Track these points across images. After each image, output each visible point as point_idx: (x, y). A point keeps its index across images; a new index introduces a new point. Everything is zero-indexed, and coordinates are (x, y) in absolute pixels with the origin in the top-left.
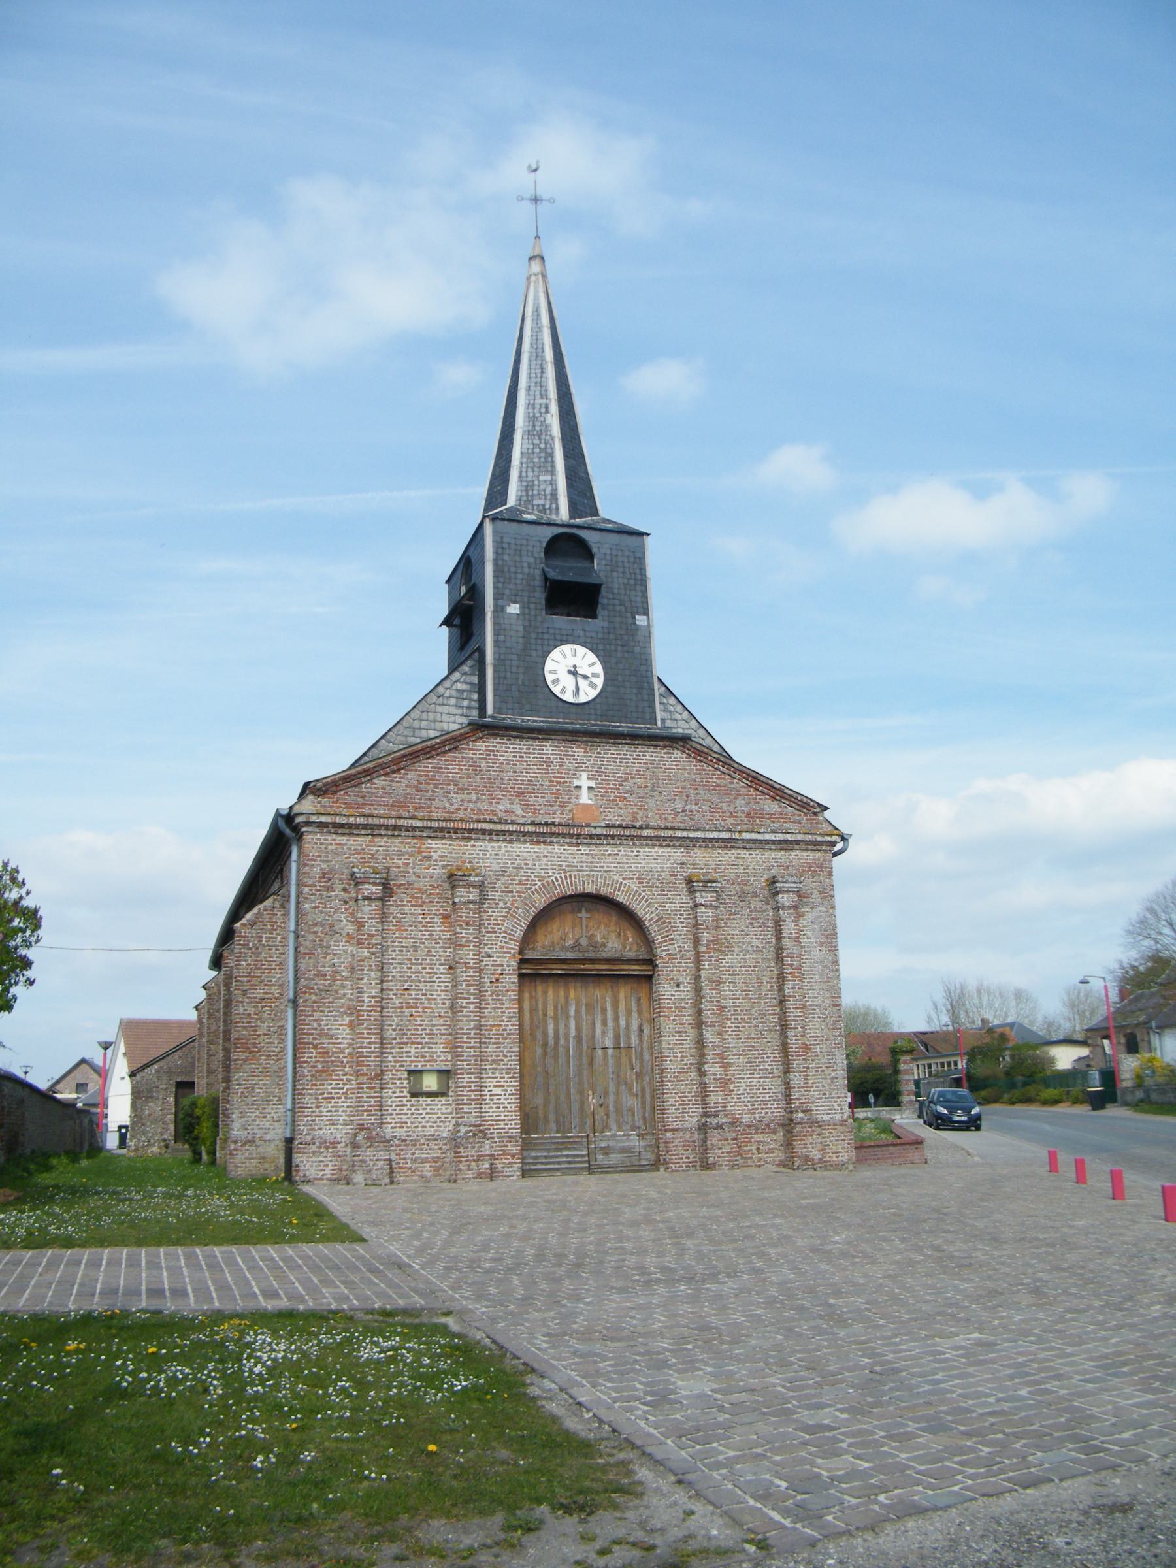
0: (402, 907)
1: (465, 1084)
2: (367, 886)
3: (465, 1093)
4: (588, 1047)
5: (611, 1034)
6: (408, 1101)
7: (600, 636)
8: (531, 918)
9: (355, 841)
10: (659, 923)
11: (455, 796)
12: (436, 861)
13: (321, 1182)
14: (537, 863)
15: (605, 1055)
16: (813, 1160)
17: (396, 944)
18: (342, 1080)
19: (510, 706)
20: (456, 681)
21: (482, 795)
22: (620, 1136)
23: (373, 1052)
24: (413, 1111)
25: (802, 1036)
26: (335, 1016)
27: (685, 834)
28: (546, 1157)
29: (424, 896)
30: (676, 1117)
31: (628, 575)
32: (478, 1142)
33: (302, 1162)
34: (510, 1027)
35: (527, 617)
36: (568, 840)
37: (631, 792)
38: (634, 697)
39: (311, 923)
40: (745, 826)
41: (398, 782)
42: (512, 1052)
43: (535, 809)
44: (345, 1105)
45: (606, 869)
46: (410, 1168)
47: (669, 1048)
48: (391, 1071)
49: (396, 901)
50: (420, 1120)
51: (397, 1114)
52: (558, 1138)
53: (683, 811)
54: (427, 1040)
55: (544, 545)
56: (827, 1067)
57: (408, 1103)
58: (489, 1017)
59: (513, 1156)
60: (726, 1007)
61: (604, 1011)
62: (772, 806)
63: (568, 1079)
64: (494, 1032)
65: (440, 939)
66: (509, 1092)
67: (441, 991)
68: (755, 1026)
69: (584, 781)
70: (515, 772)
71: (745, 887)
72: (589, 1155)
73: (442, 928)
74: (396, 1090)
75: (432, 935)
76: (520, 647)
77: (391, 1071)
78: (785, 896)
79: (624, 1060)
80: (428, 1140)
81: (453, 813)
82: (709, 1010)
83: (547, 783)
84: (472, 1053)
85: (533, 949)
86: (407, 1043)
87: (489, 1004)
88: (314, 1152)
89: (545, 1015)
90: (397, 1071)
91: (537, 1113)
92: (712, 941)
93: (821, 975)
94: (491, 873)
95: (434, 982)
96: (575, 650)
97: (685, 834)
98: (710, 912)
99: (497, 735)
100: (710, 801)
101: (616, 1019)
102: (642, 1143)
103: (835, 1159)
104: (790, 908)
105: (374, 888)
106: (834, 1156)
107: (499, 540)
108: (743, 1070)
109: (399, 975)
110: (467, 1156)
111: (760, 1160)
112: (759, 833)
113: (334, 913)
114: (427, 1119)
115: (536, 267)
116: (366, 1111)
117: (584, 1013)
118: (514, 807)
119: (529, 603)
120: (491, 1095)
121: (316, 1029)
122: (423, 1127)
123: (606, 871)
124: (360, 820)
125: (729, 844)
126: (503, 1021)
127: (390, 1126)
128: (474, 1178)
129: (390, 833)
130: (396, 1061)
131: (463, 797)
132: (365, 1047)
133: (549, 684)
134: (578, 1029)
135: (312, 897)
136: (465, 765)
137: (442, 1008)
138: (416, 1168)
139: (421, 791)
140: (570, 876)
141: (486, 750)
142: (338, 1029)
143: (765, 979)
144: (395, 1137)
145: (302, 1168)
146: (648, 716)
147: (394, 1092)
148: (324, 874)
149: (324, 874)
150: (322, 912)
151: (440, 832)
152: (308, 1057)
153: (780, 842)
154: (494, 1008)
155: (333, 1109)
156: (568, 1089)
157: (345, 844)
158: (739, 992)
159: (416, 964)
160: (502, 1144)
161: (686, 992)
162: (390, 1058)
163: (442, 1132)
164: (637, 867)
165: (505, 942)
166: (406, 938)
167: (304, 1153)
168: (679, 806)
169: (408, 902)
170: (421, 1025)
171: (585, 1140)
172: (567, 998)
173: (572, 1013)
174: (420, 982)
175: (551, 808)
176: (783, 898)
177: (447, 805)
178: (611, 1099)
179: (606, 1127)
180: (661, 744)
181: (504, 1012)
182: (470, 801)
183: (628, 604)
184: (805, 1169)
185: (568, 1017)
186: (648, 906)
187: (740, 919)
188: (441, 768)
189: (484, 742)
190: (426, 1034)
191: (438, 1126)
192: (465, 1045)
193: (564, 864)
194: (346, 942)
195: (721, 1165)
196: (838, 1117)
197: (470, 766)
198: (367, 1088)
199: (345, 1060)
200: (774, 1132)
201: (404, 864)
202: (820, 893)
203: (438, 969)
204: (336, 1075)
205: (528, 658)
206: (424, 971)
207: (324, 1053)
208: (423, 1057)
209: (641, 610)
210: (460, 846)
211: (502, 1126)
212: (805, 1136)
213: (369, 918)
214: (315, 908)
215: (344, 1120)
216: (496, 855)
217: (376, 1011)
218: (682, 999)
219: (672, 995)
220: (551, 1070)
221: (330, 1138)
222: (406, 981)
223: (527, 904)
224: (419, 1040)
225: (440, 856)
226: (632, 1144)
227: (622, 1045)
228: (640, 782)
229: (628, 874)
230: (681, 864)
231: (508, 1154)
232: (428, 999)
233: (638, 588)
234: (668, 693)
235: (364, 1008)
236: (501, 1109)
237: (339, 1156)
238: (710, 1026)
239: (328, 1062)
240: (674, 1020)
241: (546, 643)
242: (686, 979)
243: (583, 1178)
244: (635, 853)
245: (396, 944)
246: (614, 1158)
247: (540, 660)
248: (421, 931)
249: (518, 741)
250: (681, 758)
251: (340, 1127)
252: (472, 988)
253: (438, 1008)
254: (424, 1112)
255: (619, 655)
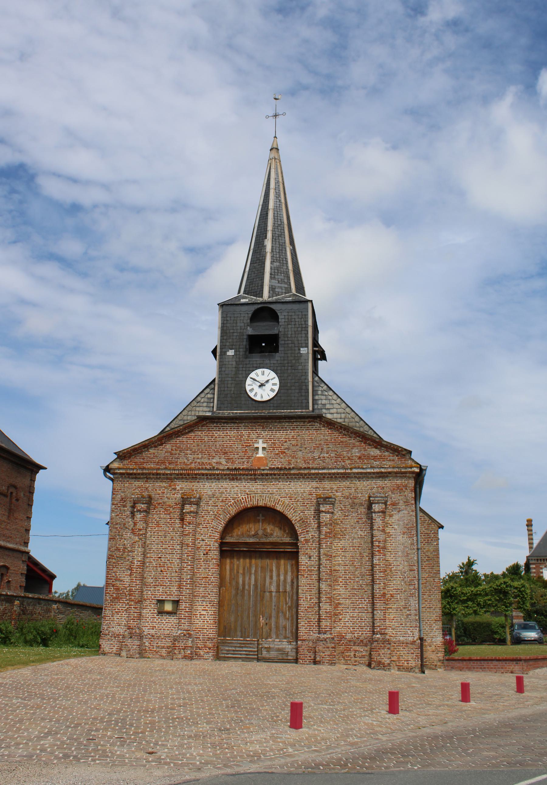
0: (156, 515)
1: (183, 608)
2: (140, 505)
3: (183, 613)
4: (261, 591)
5: (275, 584)
6: (157, 615)
7: (279, 362)
8: (227, 520)
9: (138, 481)
10: (301, 522)
11: (190, 456)
12: (178, 490)
13: (111, 654)
14: (232, 490)
15: (271, 596)
16: (384, 664)
17: (156, 534)
18: (125, 603)
19: (226, 406)
20: (207, 393)
21: (204, 455)
22: (277, 641)
23: (137, 589)
24: (159, 621)
25: (383, 589)
26: (123, 570)
27: (317, 471)
28: (234, 651)
29: (171, 509)
30: (305, 633)
31: (297, 326)
32: (186, 639)
33: (103, 643)
34: (213, 579)
35: (238, 356)
36: (249, 477)
37: (288, 449)
38: (296, 395)
39: (114, 523)
40: (357, 465)
41: (161, 450)
42: (213, 592)
43: (233, 461)
44: (126, 616)
45: (271, 492)
46: (155, 651)
47: (303, 593)
48: (149, 599)
49: (157, 512)
50: (162, 626)
51: (151, 622)
52: (241, 640)
53: (319, 458)
54: (168, 584)
55: (250, 315)
56: (404, 608)
57: (157, 617)
58: (202, 573)
59: (210, 648)
60: (339, 570)
61: (271, 571)
62: (375, 452)
63: (249, 608)
64: (204, 581)
65: (178, 531)
66: (210, 613)
67: (177, 558)
68: (357, 582)
69: (260, 445)
70: (223, 441)
71: (355, 500)
72: (258, 651)
73: (180, 526)
74: (149, 611)
75: (174, 529)
76: (233, 373)
77: (149, 599)
78: (377, 505)
79: (282, 598)
80: (165, 636)
81: (189, 465)
82: (324, 572)
83: (241, 447)
84: (188, 592)
85: (232, 536)
86: (158, 585)
87: (202, 566)
88: (108, 639)
89: (238, 572)
90: (152, 599)
91: (231, 626)
92: (328, 532)
93: (403, 552)
94: (207, 496)
95: (174, 554)
96: (264, 372)
97: (317, 471)
98: (328, 516)
99: (214, 422)
100: (335, 451)
101: (278, 575)
102: (290, 647)
103: (406, 664)
104: (379, 512)
105: (143, 506)
106: (406, 662)
107: (225, 316)
108: (348, 608)
109: (156, 550)
110: (179, 646)
111: (356, 661)
112: (363, 468)
113: (126, 518)
114: (166, 626)
115: (274, 154)
116: (132, 619)
117: (259, 572)
118: (222, 460)
119: (239, 348)
120: (200, 615)
121: (114, 577)
122: (164, 629)
123: (271, 494)
124: (139, 471)
125: (345, 476)
126: (209, 575)
127: (147, 628)
128: (182, 658)
129: (155, 477)
130: (152, 595)
131: (194, 456)
132: (134, 587)
133: (248, 391)
134: (256, 581)
135: (116, 510)
136: (196, 440)
137: (177, 568)
138: (158, 651)
139: (173, 454)
140: (250, 497)
141: (208, 431)
142: (125, 577)
143: (365, 554)
144: (149, 634)
145: (102, 647)
146: (304, 405)
147: (150, 611)
148: (122, 498)
149: (122, 498)
150: (120, 518)
151: (182, 477)
152: (110, 591)
153: (378, 473)
154: (205, 568)
155: (120, 618)
156: (249, 614)
157: (133, 483)
158: (348, 562)
159: (165, 544)
160: (204, 641)
161: (314, 561)
162: (149, 593)
163: (174, 633)
164: (289, 491)
165: (212, 533)
166: (161, 531)
167: (104, 639)
168: (316, 455)
169: (163, 512)
170: (166, 576)
171: (256, 642)
172: (250, 563)
173: (253, 571)
174: (167, 553)
175: (241, 460)
176: (375, 506)
177: (186, 461)
178: (273, 620)
179: (269, 636)
180: (307, 420)
181: (209, 571)
182: (198, 458)
183: (296, 342)
184: (378, 669)
185: (250, 574)
186: (294, 512)
187: (351, 519)
188: (184, 442)
189: (207, 426)
190: (168, 581)
191: (172, 630)
192: (184, 587)
193: (247, 490)
194: (131, 533)
195: (324, 662)
196: (411, 639)
197: (199, 440)
198: (134, 608)
199: (127, 593)
200: (366, 646)
201: (162, 492)
202: (405, 502)
203: (176, 547)
204: (122, 600)
205: (237, 379)
206: (169, 548)
207: (117, 588)
208: (166, 593)
209: (304, 345)
210: (192, 482)
211: (205, 632)
212: (379, 649)
213: (139, 521)
214: (117, 515)
215: (125, 624)
216: (210, 486)
217: (140, 568)
218: (312, 565)
219: (306, 563)
220: (239, 602)
221: (117, 632)
222: (160, 553)
223: (225, 513)
224: (165, 584)
225: (181, 488)
226: (284, 647)
227: (281, 590)
228: (293, 443)
229: (284, 495)
230: (316, 488)
231: (207, 647)
232: (171, 563)
233: (303, 332)
234: (329, 389)
235: (135, 567)
236: (205, 623)
237: (120, 642)
238: (324, 581)
239: (119, 593)
240: (307, 577)
241: (286, 359)
242: (315, 554)
243: (255, 663)
244: (289, 483)
245: (156, 534)
246: (273, 654)
247: (244, 379)
248: (169, 527)
249: (225, 425)
250: (319, 427)
251: (123, 627)
252: (190, 557)
253: (175, 567)
254: (165, 622)
255: (289, 371)
